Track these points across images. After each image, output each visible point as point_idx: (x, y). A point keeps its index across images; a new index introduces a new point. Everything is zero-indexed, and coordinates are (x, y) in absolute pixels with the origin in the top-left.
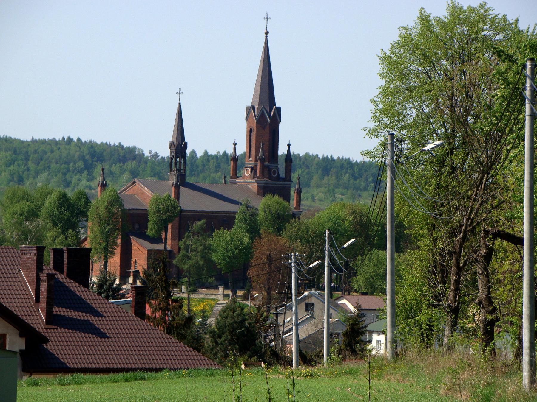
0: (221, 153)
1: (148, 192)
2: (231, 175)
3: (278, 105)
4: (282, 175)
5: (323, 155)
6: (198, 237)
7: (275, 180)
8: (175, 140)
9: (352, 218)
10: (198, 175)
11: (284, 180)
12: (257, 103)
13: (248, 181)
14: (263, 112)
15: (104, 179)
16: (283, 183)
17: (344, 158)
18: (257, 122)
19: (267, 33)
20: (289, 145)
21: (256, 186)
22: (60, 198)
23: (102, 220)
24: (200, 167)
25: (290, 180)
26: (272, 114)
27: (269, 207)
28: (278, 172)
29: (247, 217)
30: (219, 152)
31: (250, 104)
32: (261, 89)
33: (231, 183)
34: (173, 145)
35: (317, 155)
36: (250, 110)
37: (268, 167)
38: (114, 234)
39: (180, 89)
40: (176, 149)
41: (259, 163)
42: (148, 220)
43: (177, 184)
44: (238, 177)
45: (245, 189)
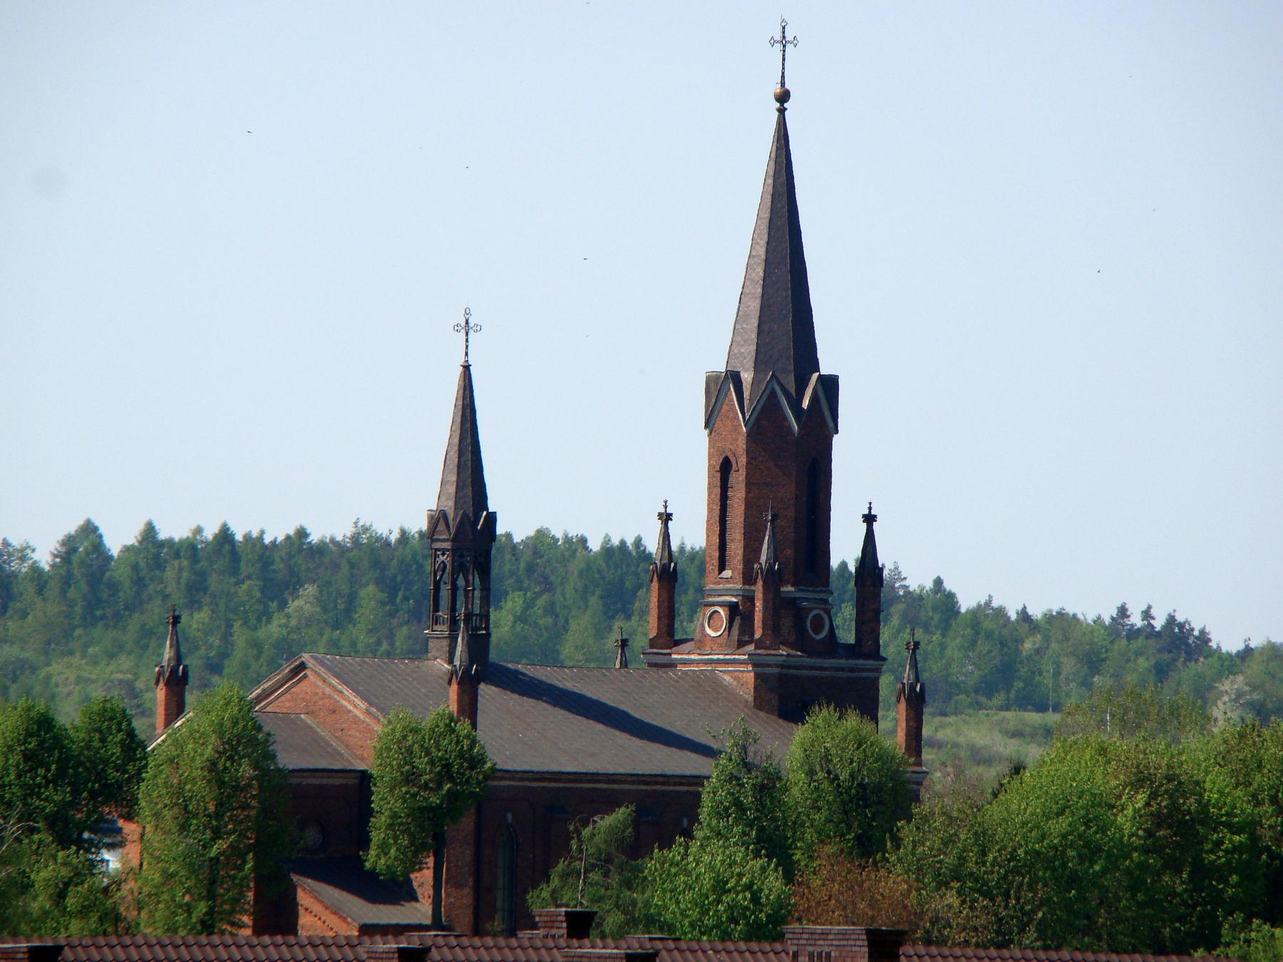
0: (210, 533)
1: (354, 705)
2: (653, 634)
3: (825, 369)
4: (847, 635)
5: (607, 540)
6: (606, 875)
7: (819, 655)
8: (449, 506)
9: (1141, 799)
10: (117, 617)
11: (851, 651)
12: (750, 363)
13: (718, 661)
14: (773, 395)
15: (179, 658)
16: (852, 662)
17: (688, 548)
18: (749, 434)
19: (783, 97)
20: (870, 519)
21: (749, 676)
22: (29, 734)
23: (195, 816)
24: (127, 591)
25: (875, 654)
26: (805, 404)
27: (827, 758)
28: (831, 625)
29: (748, 800)
30: (199, 530)
31: (720, 365)
32: (762, 307)
33: (650, 665)
34: (442, 526)
35: (583, 541)
36: (721, 388)
37: (792, 602)
38: (240, 868)
39: (467, 312)
40: (453, 541)
41: (758, 590)
42: (371, 813)
43: (467, 671)
44: (677, 643)
45: (708, 687)
